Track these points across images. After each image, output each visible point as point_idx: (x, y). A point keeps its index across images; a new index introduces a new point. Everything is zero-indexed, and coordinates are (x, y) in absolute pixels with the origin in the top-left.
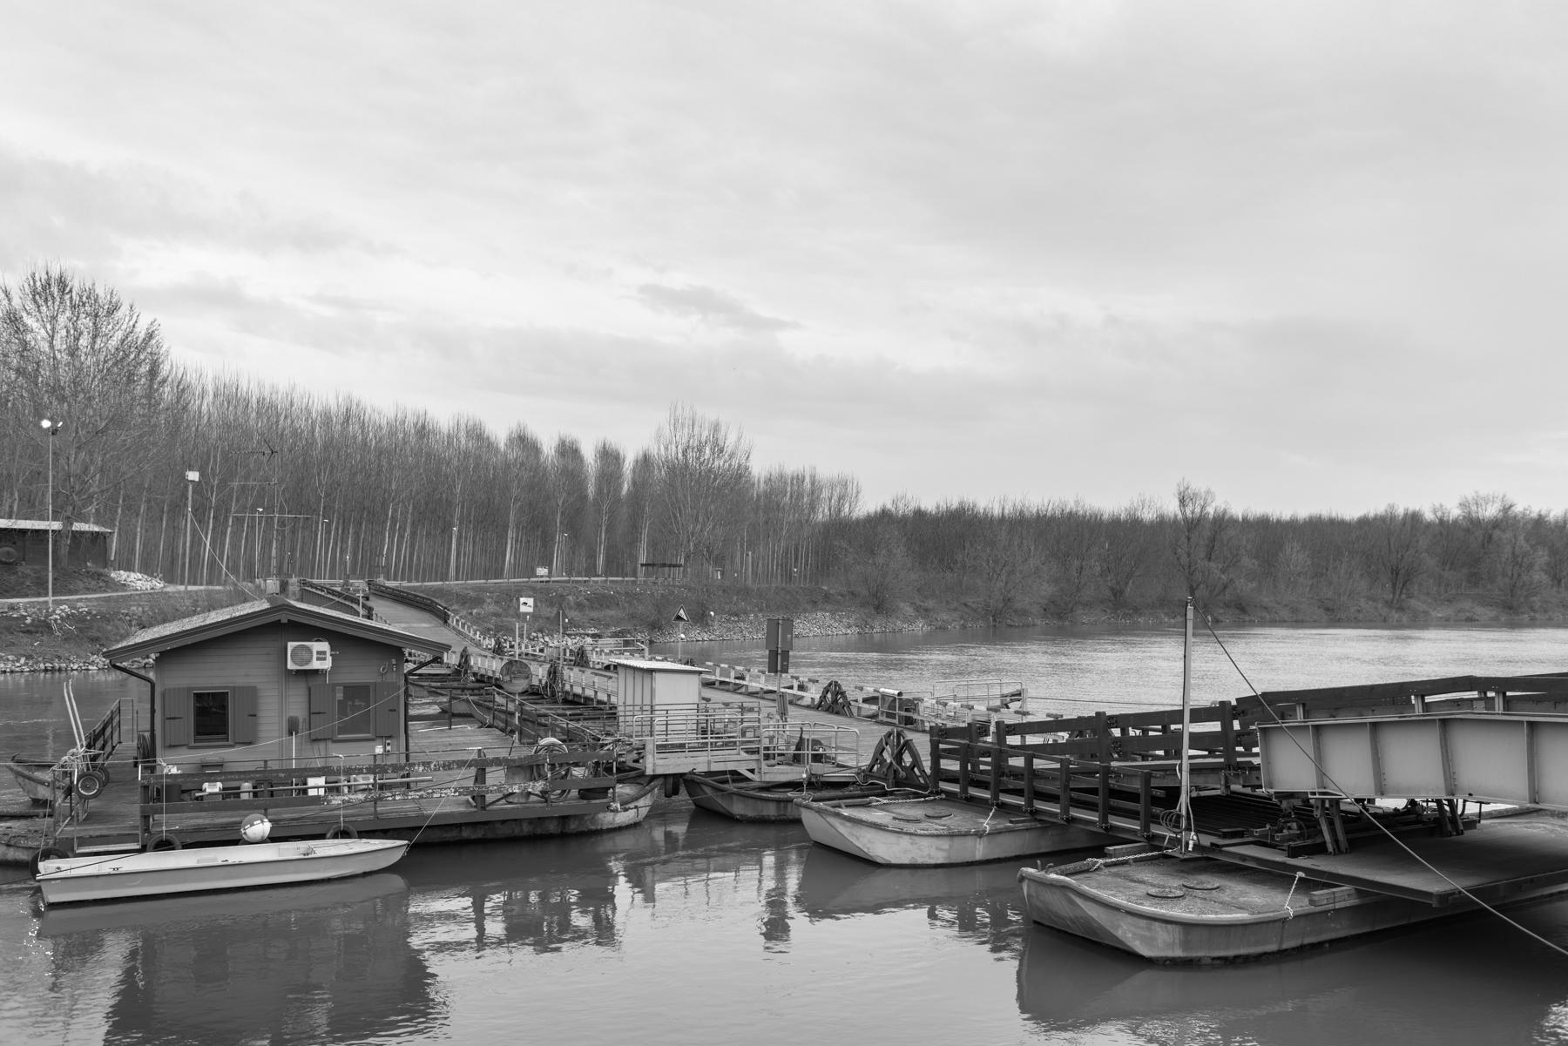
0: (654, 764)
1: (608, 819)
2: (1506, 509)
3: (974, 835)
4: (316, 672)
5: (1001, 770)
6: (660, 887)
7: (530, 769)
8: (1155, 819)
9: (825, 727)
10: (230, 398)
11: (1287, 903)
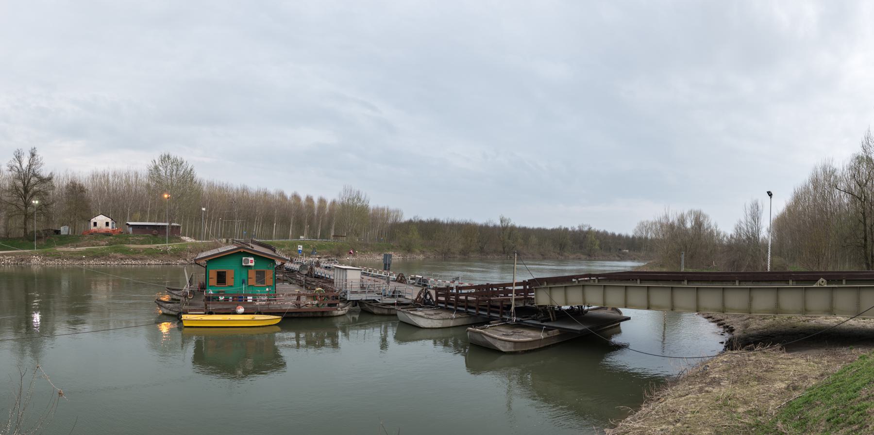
0: (349, 297)
1: (336, 313)
2: (590, 229)
3: (450, 319)
4: (250, 266)
5: (457, 299)
6: (350, 333)
7: (314, 297)
8: (504, 314)
9: (401, 287)
10: (211, 185)
11: (542, 335)
